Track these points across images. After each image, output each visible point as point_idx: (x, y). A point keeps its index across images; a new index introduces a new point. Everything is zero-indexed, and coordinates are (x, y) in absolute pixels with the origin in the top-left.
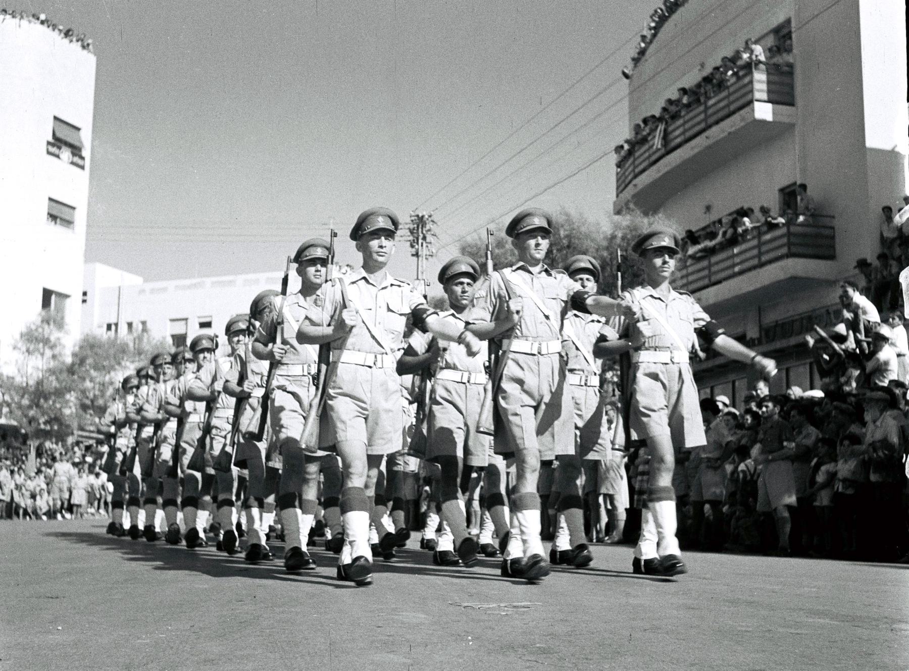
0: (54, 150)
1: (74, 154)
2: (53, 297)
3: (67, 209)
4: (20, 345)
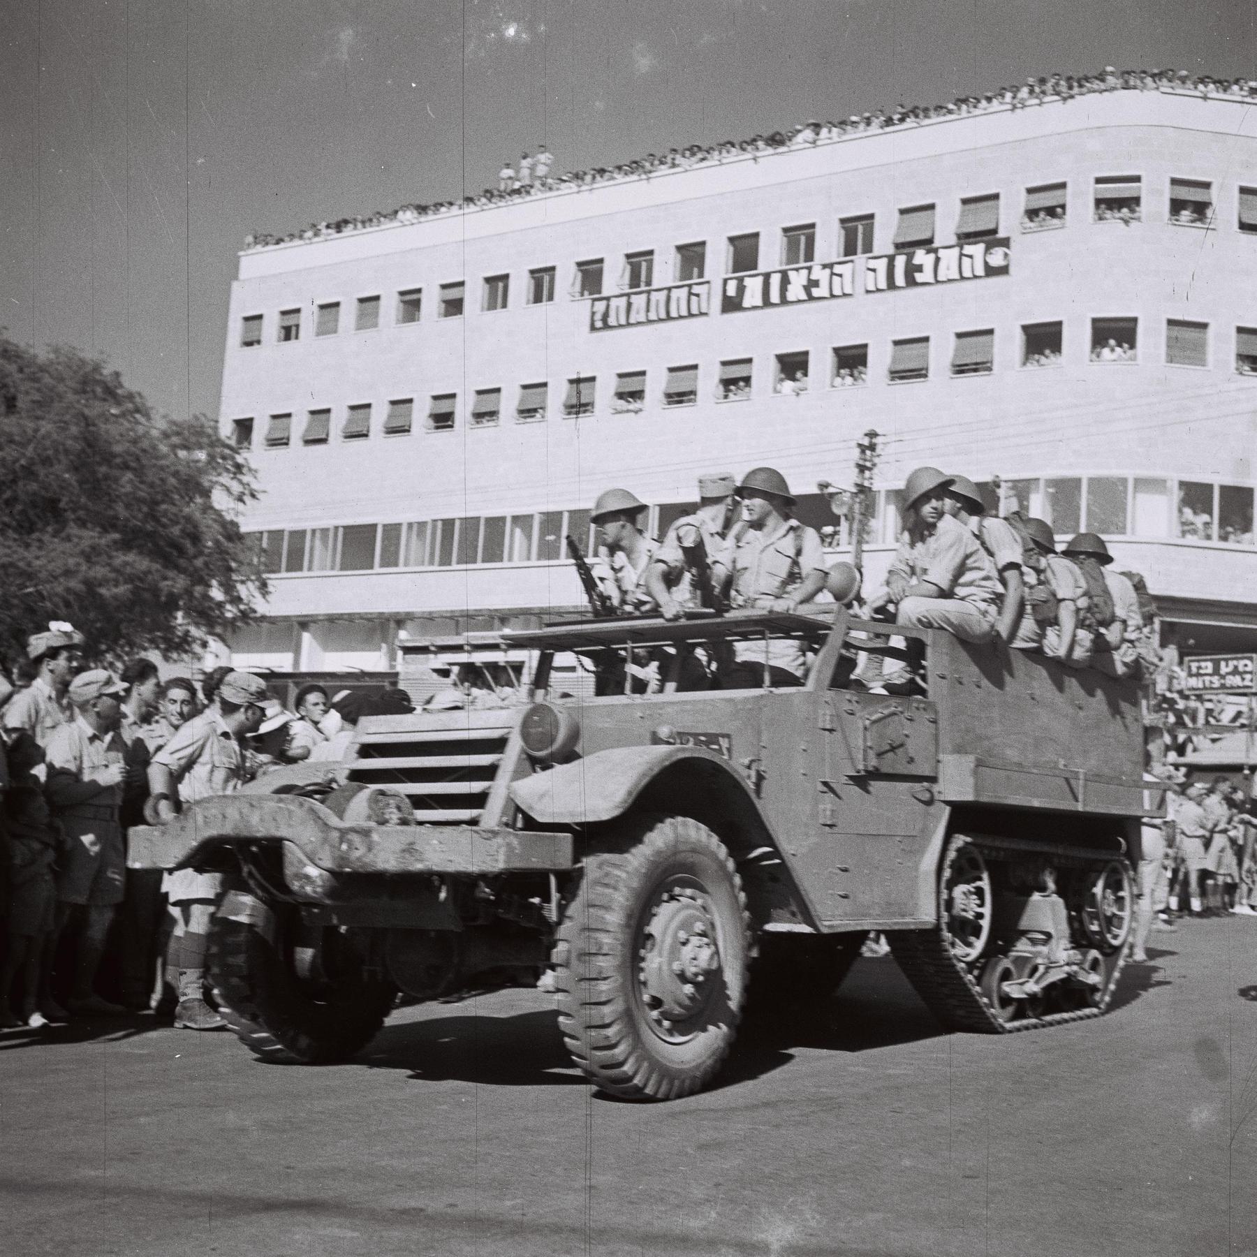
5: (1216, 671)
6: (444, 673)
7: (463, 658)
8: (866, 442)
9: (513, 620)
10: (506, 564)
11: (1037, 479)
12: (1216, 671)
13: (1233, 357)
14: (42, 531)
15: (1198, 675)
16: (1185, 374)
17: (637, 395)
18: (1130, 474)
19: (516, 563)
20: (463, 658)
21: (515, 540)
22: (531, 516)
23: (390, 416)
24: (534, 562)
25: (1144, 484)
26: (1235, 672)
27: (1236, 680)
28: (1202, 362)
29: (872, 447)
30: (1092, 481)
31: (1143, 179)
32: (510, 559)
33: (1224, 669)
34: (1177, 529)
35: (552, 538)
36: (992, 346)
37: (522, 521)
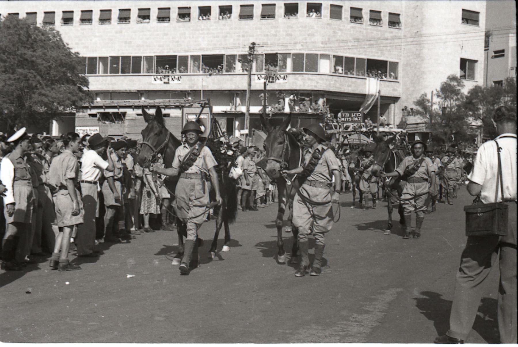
2: (467, 63)
3: (473, 14)
4: (440, 94)
5: (350, 116)
6: (94, 116)
7: (102, 111)
8: (252, 46)
9: (101, 94)
10: (97, 74)
11: (290, 53)
12: (350, 116)
13: (349, 17)
14: (459, 106)
15: (344, 117)
16: (335, 22)
17: (148, 17)
18: (319, 53)
19: (101, 74)
20: (102, 111)
21: (100, 67)
22: (107, 58)
23: (45, 18)
24: (109, 74)
25: (325, 56)
26: (356, 116)
27: (356, 119)
28: (397, 63)
29: (253, 48)
30: (307, 54)
31: (394, 31)
32: (99, 73)
33: (352, 116)
34: (333, 70)
35: (115, 66)
36: (275, 10)
37: (103, 59)
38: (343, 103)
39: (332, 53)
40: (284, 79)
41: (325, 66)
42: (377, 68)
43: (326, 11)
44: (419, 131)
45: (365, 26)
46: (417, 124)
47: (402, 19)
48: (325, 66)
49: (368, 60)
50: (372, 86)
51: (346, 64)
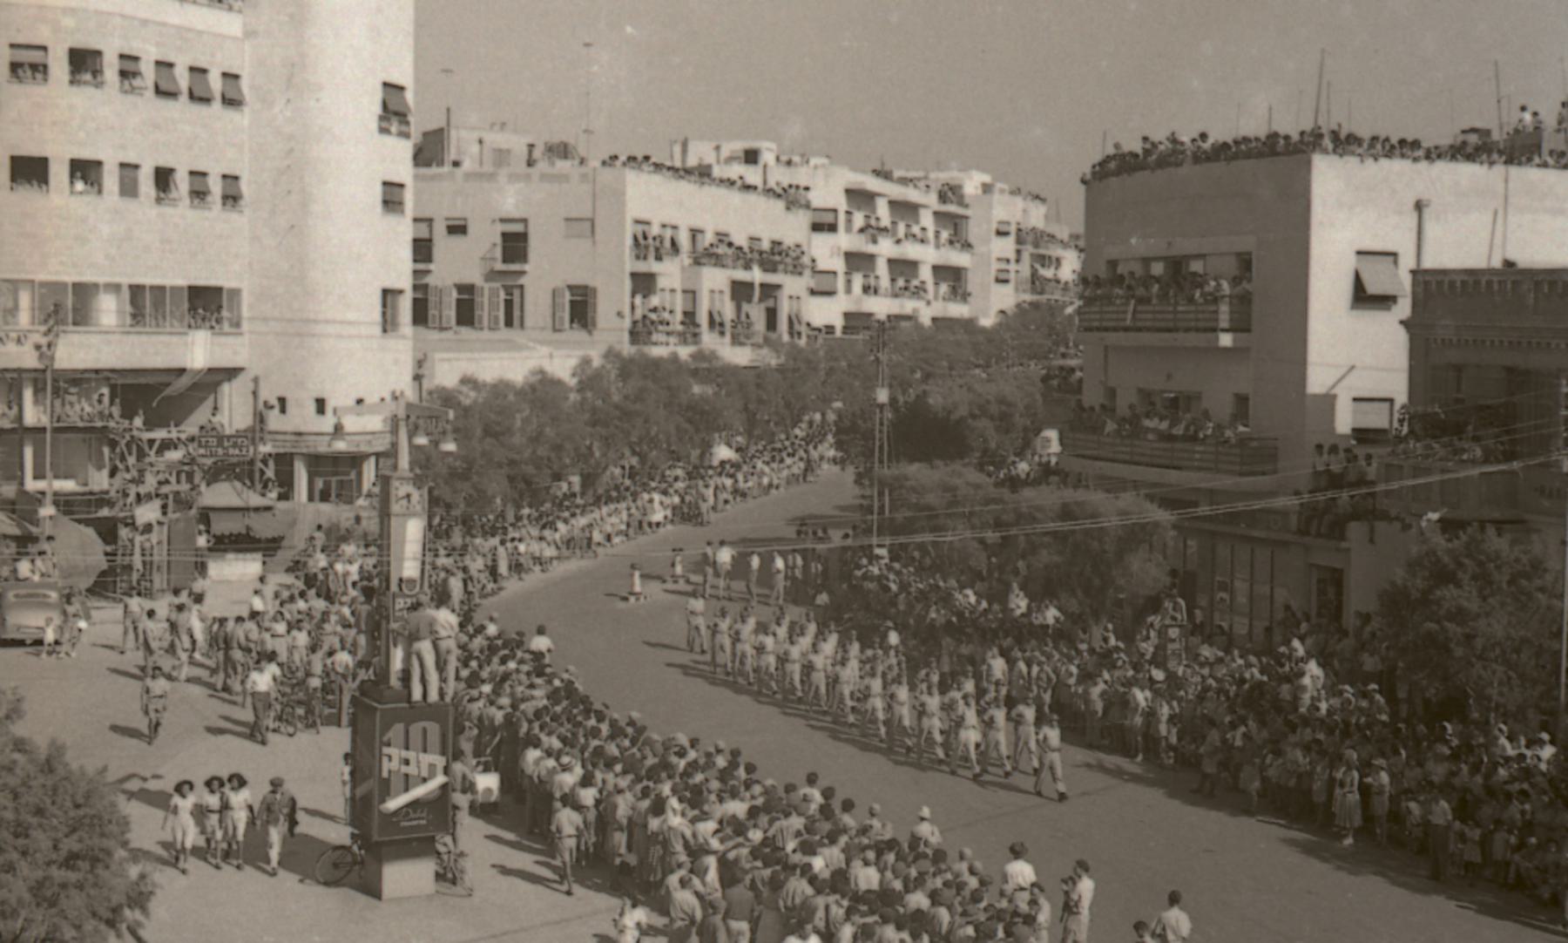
0: (384, 125)
1: (401, 122)
16: (129, 204)
38: (150, 395)
39: (125, 281)
40: (19, 341)
41: (108, 309)
42: (205, 303)
43: (111, 180)
44: (304, 451)
45: (181, 212)
46: (300, 434)
47: (245, 187)
48: (108, 309)
49: (191, 288)
50: (198, 350)
51: (145, 303)
